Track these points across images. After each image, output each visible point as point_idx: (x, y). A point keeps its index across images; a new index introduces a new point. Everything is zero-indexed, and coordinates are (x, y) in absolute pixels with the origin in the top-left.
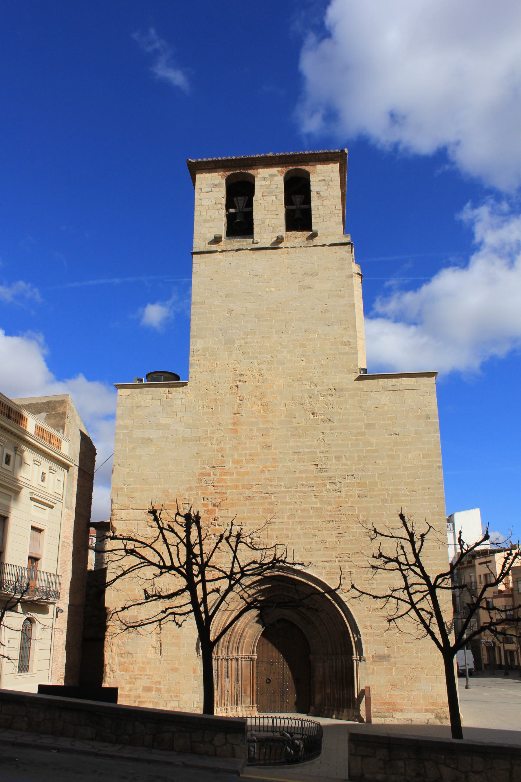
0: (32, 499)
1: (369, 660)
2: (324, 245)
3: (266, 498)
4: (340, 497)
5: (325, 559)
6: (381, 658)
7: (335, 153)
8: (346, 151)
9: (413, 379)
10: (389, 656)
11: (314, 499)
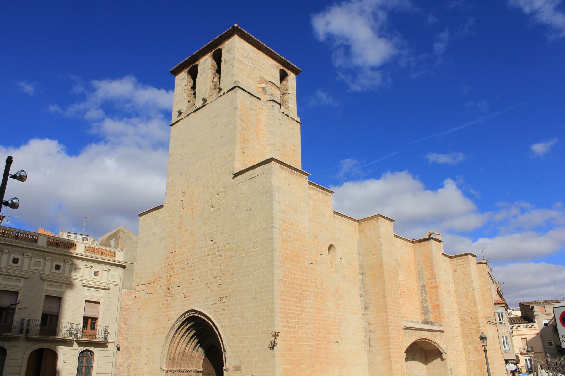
0: (84, 286)
1: (231, 370)
2: (224, 94)
3: (190, 267)
4: (222, 260)
5: (213, 303)
6: (237, 368)
7: (231, 30)
8: (236, 25)
9: (261, 167)
10: (240, 367)
11: (210, 264)
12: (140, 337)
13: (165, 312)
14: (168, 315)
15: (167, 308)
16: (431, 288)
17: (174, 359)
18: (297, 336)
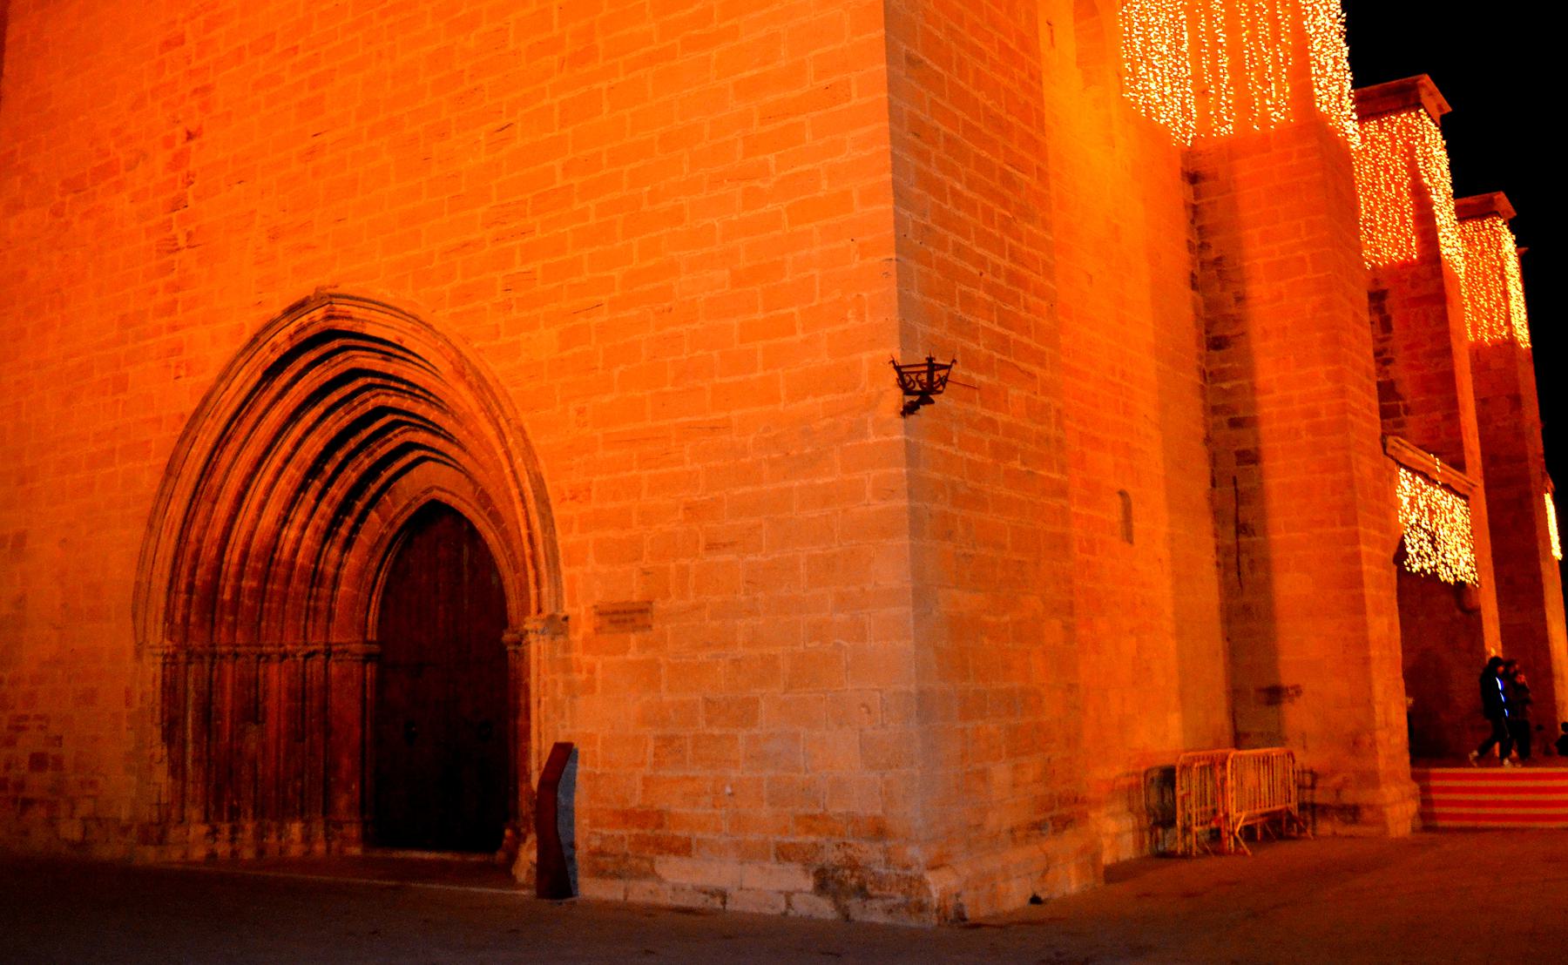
1: (582, 630)
12: (22, 482)
13: (157, 331)
14: (178, 349)
15: (170, 309)
16: (1415, 302)
17: (213, 588)
18: (1001, 418)
